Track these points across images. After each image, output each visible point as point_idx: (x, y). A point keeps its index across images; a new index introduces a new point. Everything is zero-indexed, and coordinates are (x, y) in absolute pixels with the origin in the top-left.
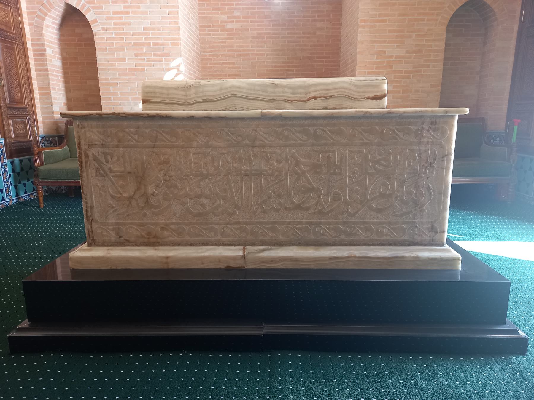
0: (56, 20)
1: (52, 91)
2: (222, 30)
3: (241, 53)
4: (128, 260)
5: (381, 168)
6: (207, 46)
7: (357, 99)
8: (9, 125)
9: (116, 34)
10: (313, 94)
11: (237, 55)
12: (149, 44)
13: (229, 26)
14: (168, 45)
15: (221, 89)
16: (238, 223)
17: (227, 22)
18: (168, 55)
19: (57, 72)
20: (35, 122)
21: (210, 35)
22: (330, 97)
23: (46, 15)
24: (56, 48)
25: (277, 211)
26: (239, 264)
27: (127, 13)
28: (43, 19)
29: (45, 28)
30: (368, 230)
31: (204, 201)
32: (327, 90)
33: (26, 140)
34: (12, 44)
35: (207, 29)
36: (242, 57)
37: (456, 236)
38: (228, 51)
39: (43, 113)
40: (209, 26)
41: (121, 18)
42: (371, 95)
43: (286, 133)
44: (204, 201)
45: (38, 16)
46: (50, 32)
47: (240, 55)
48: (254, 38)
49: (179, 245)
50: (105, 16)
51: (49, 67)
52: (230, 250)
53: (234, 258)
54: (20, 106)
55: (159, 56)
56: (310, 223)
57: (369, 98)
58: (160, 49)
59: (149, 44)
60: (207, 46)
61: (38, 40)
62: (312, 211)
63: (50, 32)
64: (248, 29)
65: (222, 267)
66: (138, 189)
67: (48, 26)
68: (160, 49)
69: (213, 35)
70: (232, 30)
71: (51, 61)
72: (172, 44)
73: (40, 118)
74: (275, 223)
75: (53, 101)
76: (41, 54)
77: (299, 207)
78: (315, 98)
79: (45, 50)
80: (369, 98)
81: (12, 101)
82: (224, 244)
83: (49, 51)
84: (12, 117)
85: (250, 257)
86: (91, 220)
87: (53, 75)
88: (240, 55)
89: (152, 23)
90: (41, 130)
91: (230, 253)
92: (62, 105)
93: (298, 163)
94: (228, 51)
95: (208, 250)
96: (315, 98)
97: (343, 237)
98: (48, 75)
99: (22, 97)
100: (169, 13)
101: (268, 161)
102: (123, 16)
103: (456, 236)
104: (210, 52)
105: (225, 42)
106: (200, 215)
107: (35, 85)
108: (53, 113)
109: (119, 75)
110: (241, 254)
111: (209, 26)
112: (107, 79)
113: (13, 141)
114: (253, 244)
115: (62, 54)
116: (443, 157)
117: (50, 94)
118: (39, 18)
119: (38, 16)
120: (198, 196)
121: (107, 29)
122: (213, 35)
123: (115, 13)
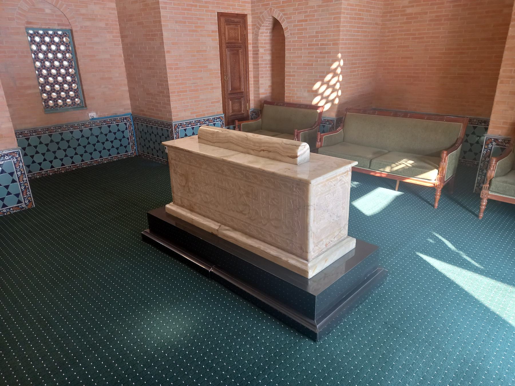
0: (269, 26)
1: (260, 79)
2: (402, 15)
3: (417, 36)
4: (181, 215)
5: (275, 203)
6: (387, 30)
7: (283, 156)
8: (228, 105)
9: (298, 38)
10: (263, 148)
11: (413, 38)
12: (318, 45)
13: (409, 11)
14: (330, 45)
15: (225, 137)
16: (219, 212)
17: (408, 7)
18: (329, 53)
19: (267, 64)
20: (248, 101)
21: (390, 20)
22: (270, 151)
23: (261, 26)
24: (268, 47)
25: (233, 211)
26: (215, 233)
27: (306, 21)
28: (259, 29)
29: (260, 35)
30: (271, 236)
31: (207, 196)
32: (269, 147)
33: (240, 113)
34: (238, 51)
35: (388, 15)
36: (417, 40)
37: (473, 262)
38: (405, 35)
39: (254, 94)
40: (391, 12)
41: (302, 25)
42: (290, 155)
43: (235, 171)
44: (207, 196)
45: (257, 27)
46: (265, 36)
47: (416, 38)
48: (431, 21)
49: (200, 214)
50: (293, 24)
51: (260, 62)
52: (215, 224)
53: (214, 229)
54: (239, 91)
55: (324, 54)
56: (247, 223)
57: (288, 156)
58: (325, 48)
59: (318, 45)
60: (387, 30)
61: (256, 43)
62: (247, 216)
63: (265, 36)
64: (427, 13)
65: (210, 232)
66: (186, 183)
67: (263, 33)
68: (325, 48)
69: (394, 20)
70: (411, 14)
71: (262, 57)
72: (334, 44)
73: (252, 97)
74: (233, 217)
75: (260, 86)
76: (256, 53)
77: (241, 212)
78: (264, 150)
79: (258, 51)
80: (288, 156)
81: (233, 89)
82: (213, 219)
83: (261, 50)
84: (232, 99)
85: (220, 231)
86: (174, 193)
87: (262, 67)
88: (416, 38)
89: (322, 28)
90: (252, 105)
91: (211, 225)
92: (267, 88)
93: (240, 189)
94: (405, 35)
95: (208, 221)
96: (264, 150)
97: (260, 236)
98: (258, 68)
99: (240, 85)
100: (334, 18)
101: (228, 184)
102: (304, 23)
103: (473, 262)
104: (388, 36)
105: (402, 27)
106: (205, 202)
107: (251, 74)
108: (259, 94)
109: (297, 68)
110: (217, 228)
111: (391, 12)
112: (290, 72)
113: (230, 115)
114: (225, 225)
115: (272, 50)
116: (305, 206)
117: (258, 81)
118: (257, 27)
119: (257, 27)
120: (206, 193)
121: (294, 34)
122: (394, 20)
123: (299, 21)
